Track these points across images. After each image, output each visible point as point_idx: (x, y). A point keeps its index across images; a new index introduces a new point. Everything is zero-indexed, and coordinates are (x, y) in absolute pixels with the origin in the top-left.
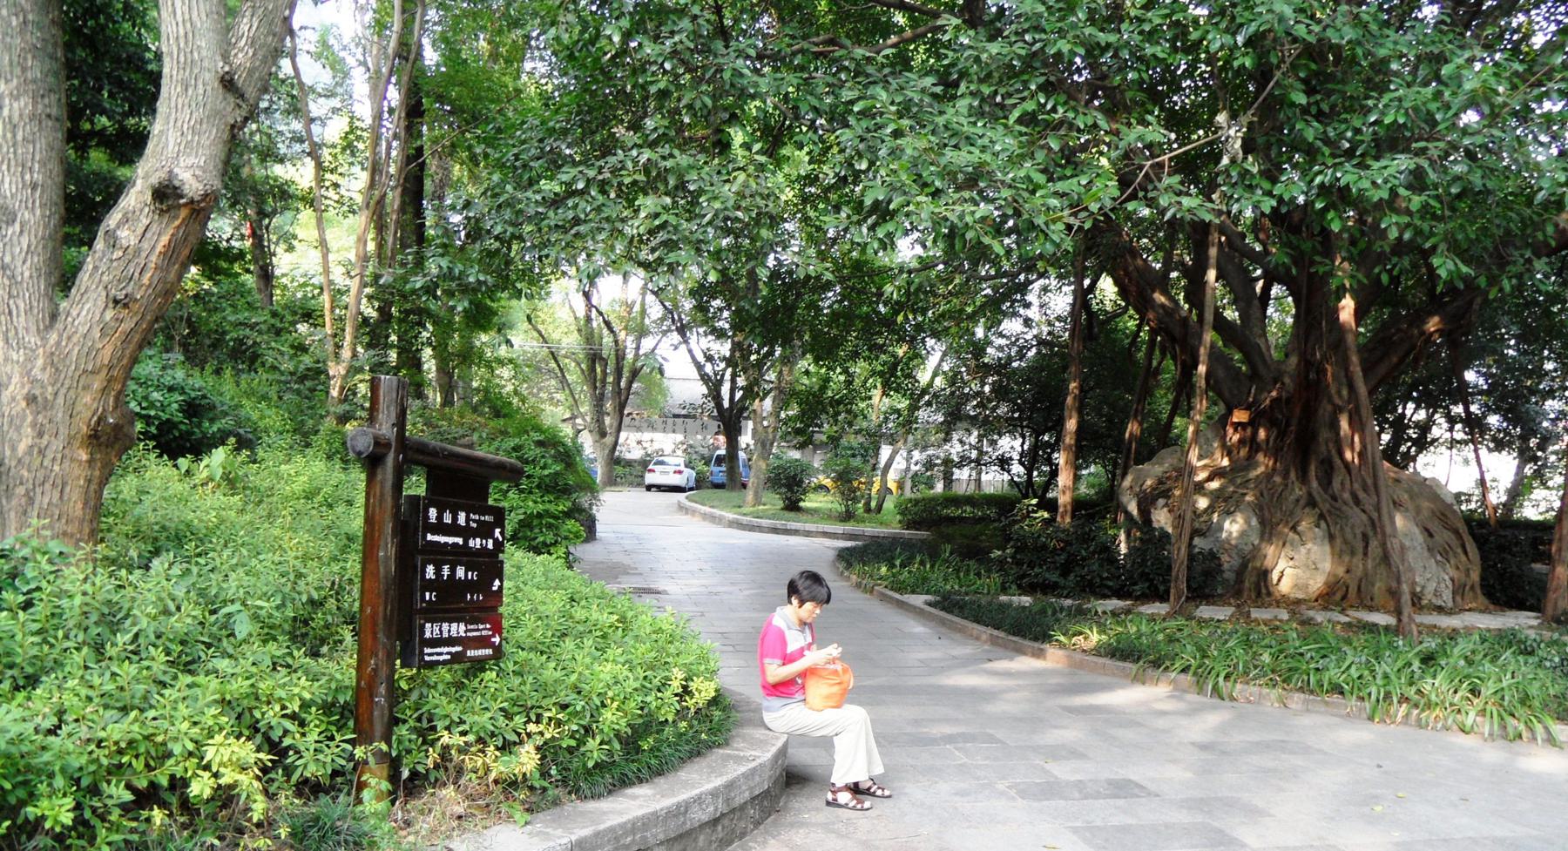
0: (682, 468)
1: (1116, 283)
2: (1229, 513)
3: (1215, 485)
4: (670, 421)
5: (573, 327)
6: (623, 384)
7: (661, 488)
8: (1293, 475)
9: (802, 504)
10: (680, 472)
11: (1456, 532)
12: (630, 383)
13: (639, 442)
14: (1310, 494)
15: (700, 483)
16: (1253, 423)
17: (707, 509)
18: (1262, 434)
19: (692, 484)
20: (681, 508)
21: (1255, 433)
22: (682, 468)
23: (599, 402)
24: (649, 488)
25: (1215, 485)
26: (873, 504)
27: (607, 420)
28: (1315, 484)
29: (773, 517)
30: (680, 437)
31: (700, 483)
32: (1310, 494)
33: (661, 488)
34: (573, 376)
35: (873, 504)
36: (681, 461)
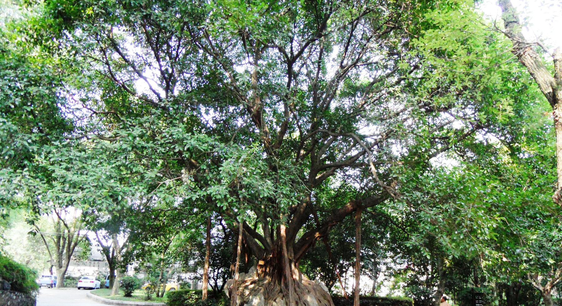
0: (94, 280)
1: (108, 221)
2: (255, 295)
3: (252, 286)
4: (93, 262)
5: (53, 226)
6: (72, 247)
7: (85, 288)
8: (277, 282)
9: (132, 294)
10: (93, 282)
11: (329, 301)
12: (74, 248)
13: (79, 270)
14: (281, 289)
15: (102, 286)
16: (265, 266)
17: (96, 296)
18: (268, 270)
19: (98, 286)
20: (88, 296)
21: (266, 269)
22: (94, 280)
23: (60, 254)
24: (79, 288)
25: (252, 286)
26: (160, 294)
27: (63, 262)
28: (283, 285)
29: (120, 299)
30: (96, 268)
31: (102, 286)
32: (281, 289)
33: (85, 288)
34: (53, 245)
35: (160, 294)
36: (94, 278)
